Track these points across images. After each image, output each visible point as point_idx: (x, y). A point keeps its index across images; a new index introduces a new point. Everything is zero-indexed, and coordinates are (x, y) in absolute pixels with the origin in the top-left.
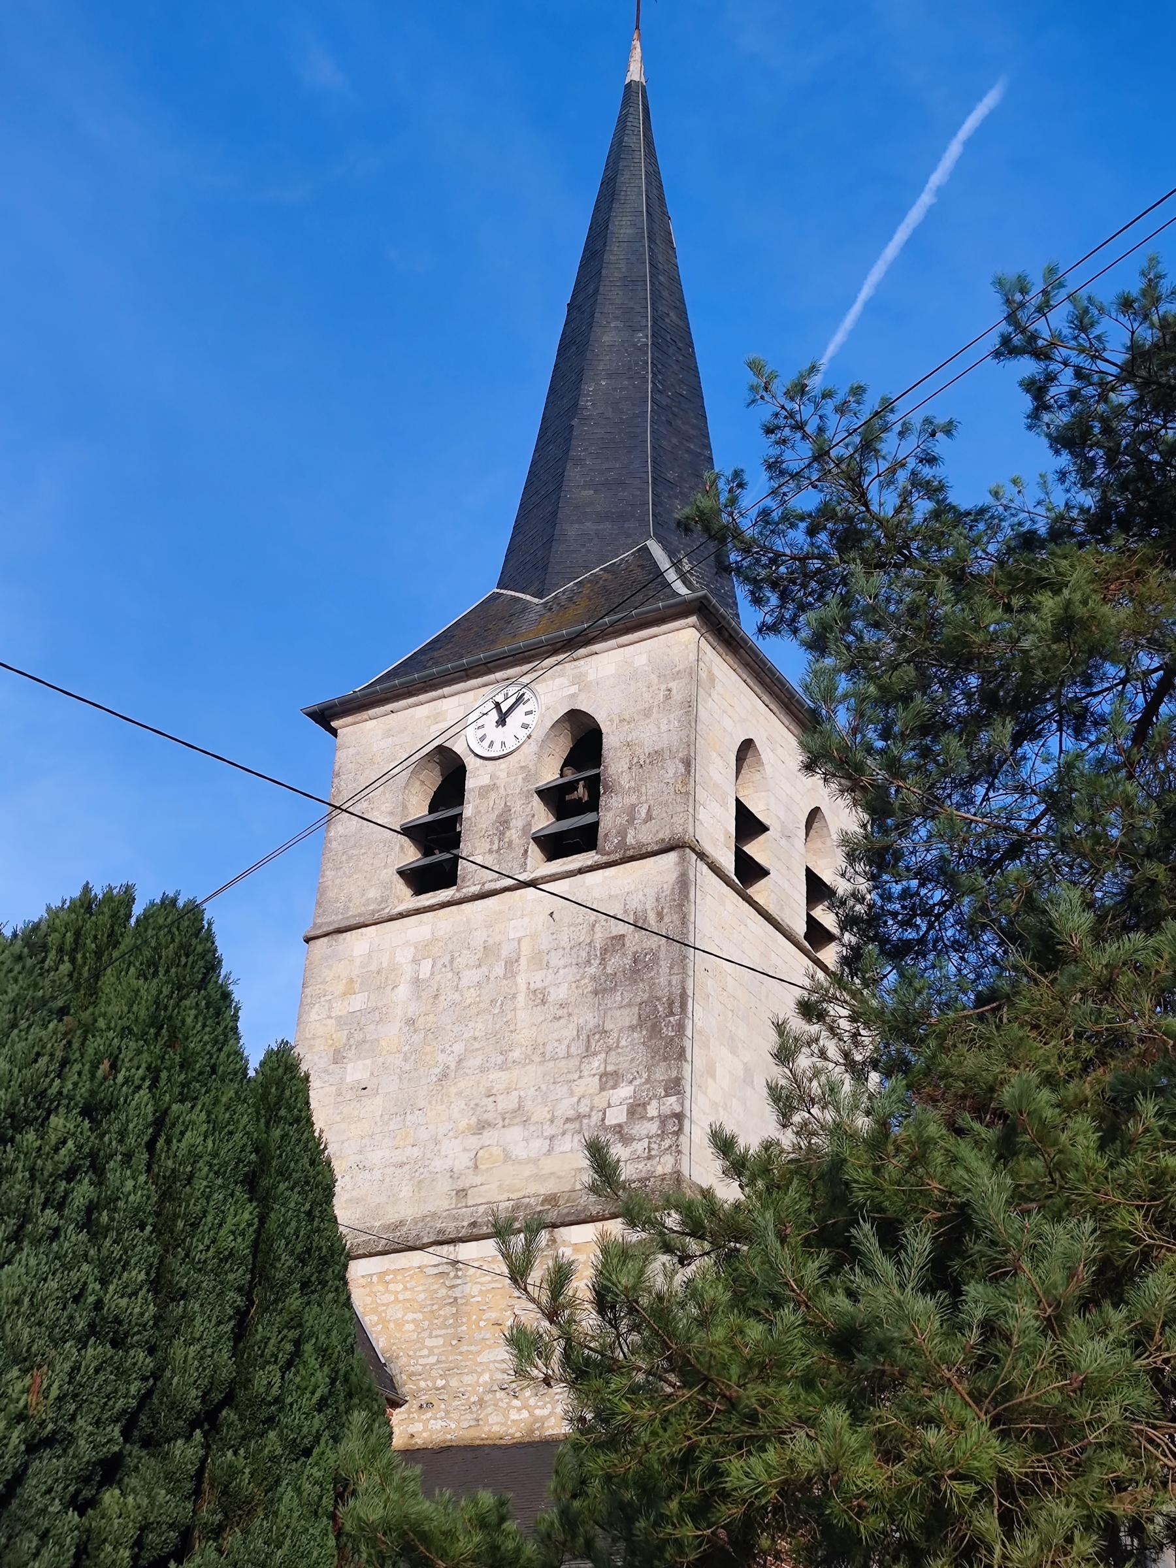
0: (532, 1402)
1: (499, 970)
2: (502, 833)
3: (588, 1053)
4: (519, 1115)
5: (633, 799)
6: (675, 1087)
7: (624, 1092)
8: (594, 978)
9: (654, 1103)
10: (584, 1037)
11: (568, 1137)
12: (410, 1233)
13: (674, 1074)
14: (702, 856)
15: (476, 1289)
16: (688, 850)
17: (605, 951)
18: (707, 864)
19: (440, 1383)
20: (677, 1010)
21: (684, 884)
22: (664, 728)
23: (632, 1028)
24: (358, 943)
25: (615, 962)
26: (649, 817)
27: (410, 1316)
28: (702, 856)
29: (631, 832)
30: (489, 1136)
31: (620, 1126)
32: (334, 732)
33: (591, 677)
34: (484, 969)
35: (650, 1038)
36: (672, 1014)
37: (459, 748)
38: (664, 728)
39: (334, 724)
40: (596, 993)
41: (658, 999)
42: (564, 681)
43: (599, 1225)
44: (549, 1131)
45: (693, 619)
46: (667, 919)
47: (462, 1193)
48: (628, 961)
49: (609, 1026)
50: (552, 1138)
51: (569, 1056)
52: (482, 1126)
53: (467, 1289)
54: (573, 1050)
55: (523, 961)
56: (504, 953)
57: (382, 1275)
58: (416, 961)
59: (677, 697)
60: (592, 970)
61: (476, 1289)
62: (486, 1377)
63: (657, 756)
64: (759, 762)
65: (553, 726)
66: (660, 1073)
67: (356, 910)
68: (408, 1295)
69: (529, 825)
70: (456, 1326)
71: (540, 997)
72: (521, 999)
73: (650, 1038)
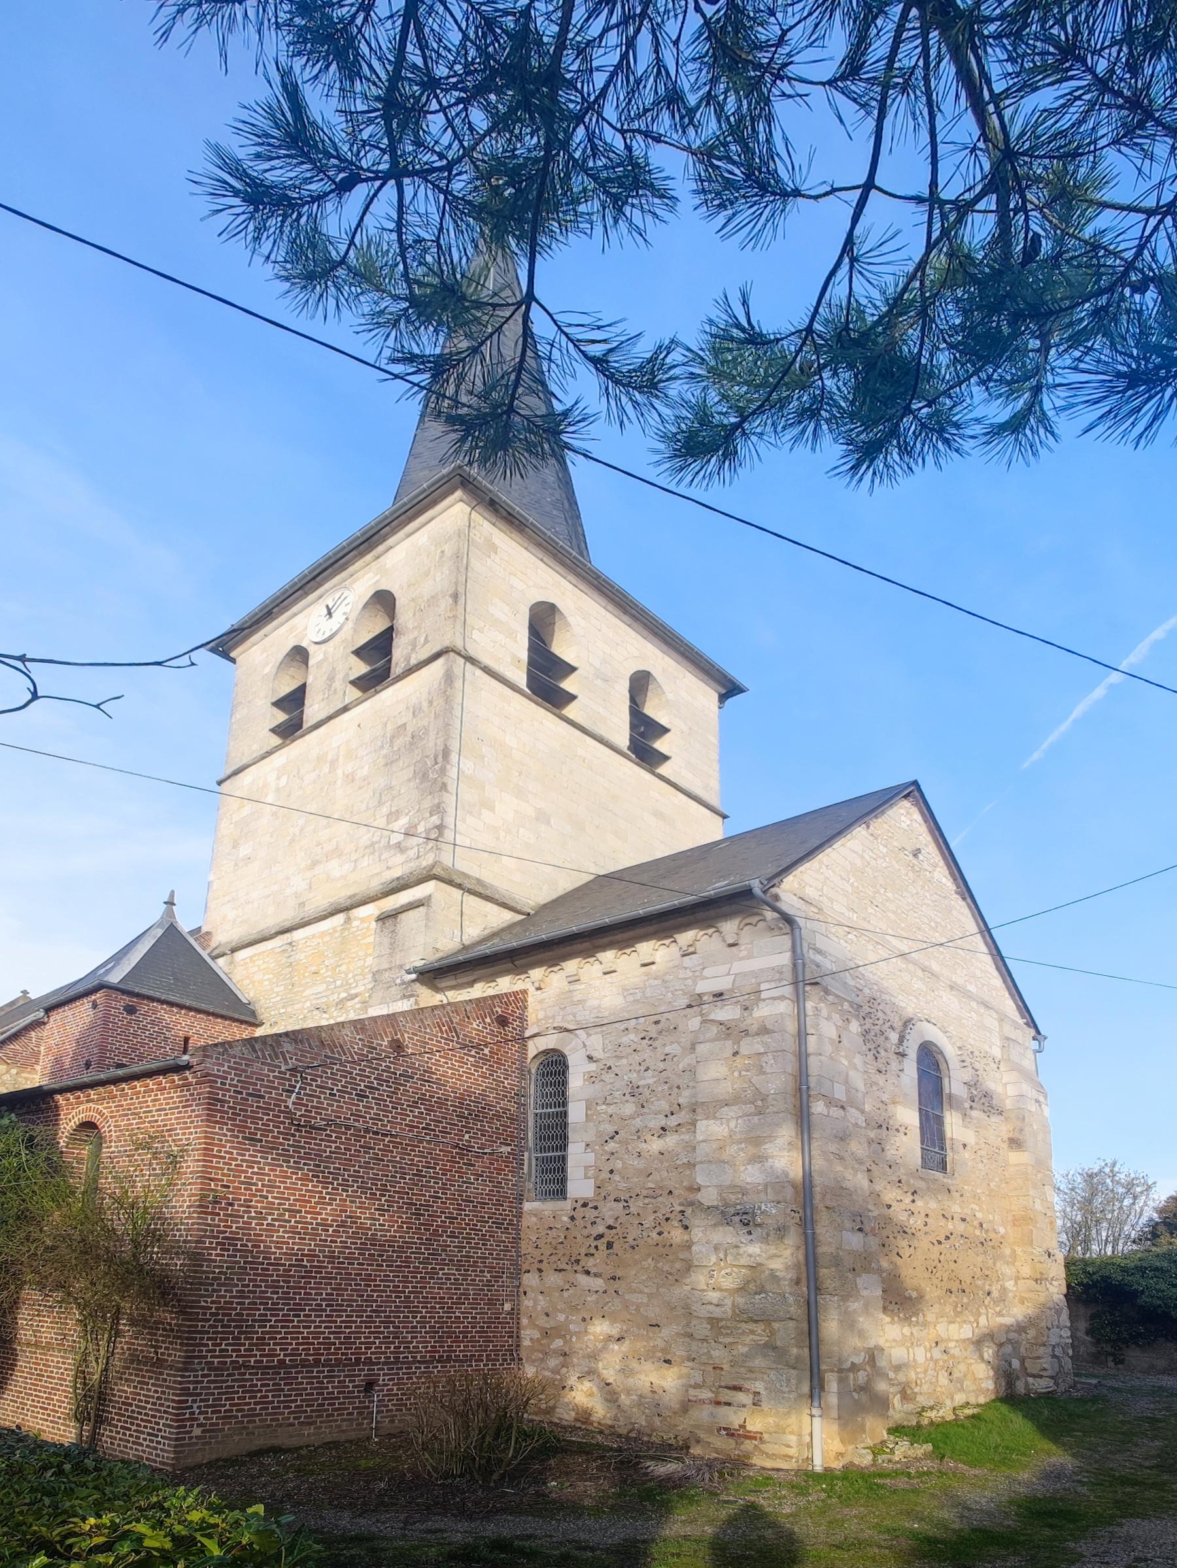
0: (335, 1014)
1: (326, 769)
2: (330, 686)
3: (380, 803)
4: (337, 852)
5: (416, 634)
6: (438, 809)
7: (402, 823)
8: (385, 756)
9: (422, 823)
10: (377, 795)
11: (366, 858)
12: (267, 933)
13: (436, 802)
14: (470, 660)
15: (302, 956)
16: (452, 654)
17: (393, 737)
18: (481, 668)
19: (282, 1011)
20: (440, 759)
21: (449, 678)
22: (438, 579)
23: (409, 780)
24: (246, 778)
25: (398, 743)
26: (426, 641)
27: (267, 977)
28: (470, 660)
29: (413, 656)
30: (319, 869)
31: (399, 843)
32: (233, 661)
33: (388, 566)
34: (317, 772)
35: (421, 783)
36: (436, 763)
37: (304, 645)
38: (438, 579)
39: (232, 655)
40: (386, 765)
41: (427, 757)
42: (371, 574)
43: (378, 903)
44: (354, 857)
45: (459, 493)
46: (435, 704)
47: (302, 904)
48: (408, 739)
49: (393, 783)
50: (356, 861)
51: (368, 808)
52: (315, 863)
53: (297, 957)
54: (371, 805)
55: (341, 759)
56: (329, 758)
57: (251, 958)
58: (278, 778)
59: (448, 553)
60: (385, 751)
61: (302, 956)
62: (308, 1004)
63: (433, 600)
64: (567, 624)
65: (365, 607)
66: (428, 803)
67: (245, 761)
68: (265, 966)
69: (347, 674)
70: (291, 978)
71: (350, 778)
72: (339, 782)
73: (421, 783)
